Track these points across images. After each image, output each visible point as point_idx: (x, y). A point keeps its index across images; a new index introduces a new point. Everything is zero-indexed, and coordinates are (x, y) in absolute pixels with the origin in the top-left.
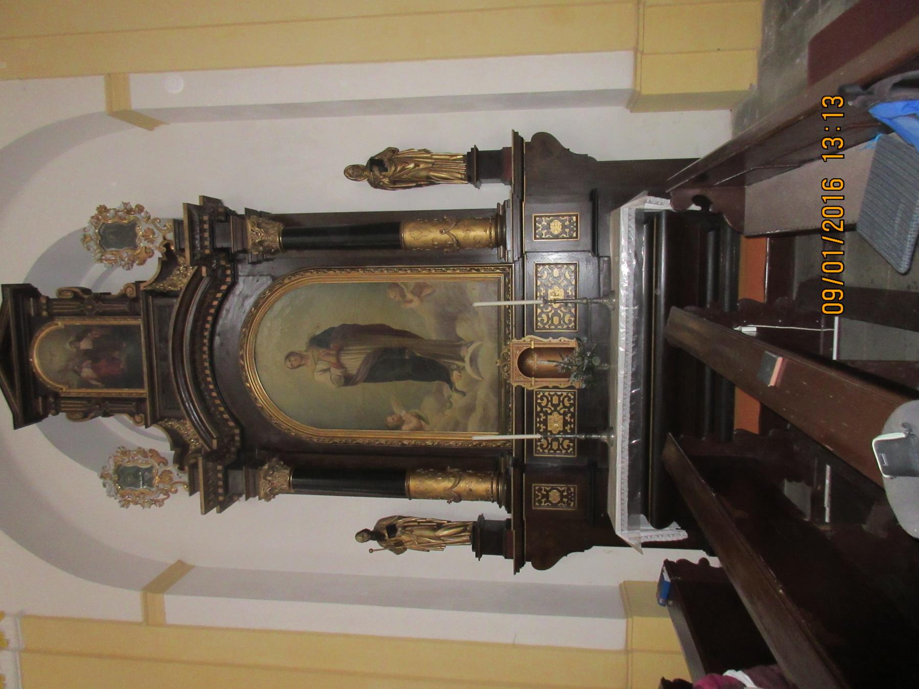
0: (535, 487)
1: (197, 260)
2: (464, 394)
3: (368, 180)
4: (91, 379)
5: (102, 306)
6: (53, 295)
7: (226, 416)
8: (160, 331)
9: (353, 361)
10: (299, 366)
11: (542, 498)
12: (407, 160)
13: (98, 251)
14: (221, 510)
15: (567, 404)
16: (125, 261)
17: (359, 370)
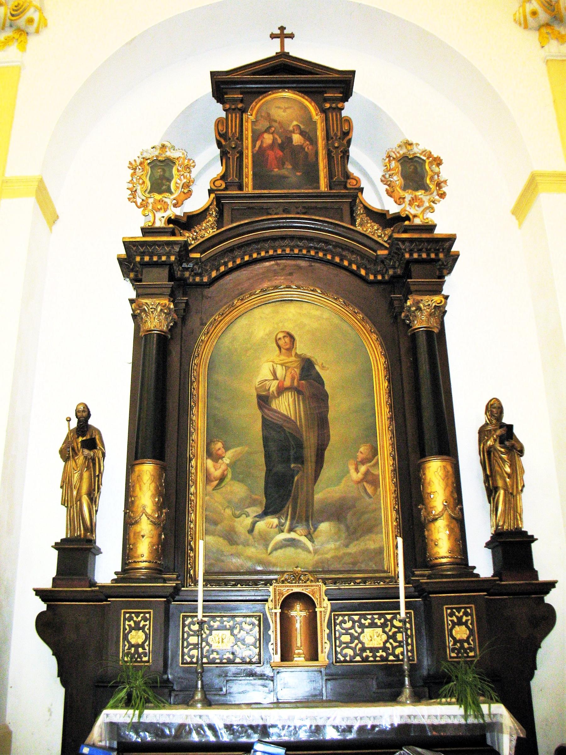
0: (149, 613)
1: (398, 244)
2: (251, 531)
3: (487, 424)
4: (262, 142)
5: (337, 156)
6: (344, 113)
7: (222, 269)
8: (316, 208)
9: (287, 404)
10: (279, 346)
11: (135, 622)
12: (513, 466)
13: (398, 155)
14: (121, 261)
15: (349, 624)
16: (389, 178)
17: (276, 411)
